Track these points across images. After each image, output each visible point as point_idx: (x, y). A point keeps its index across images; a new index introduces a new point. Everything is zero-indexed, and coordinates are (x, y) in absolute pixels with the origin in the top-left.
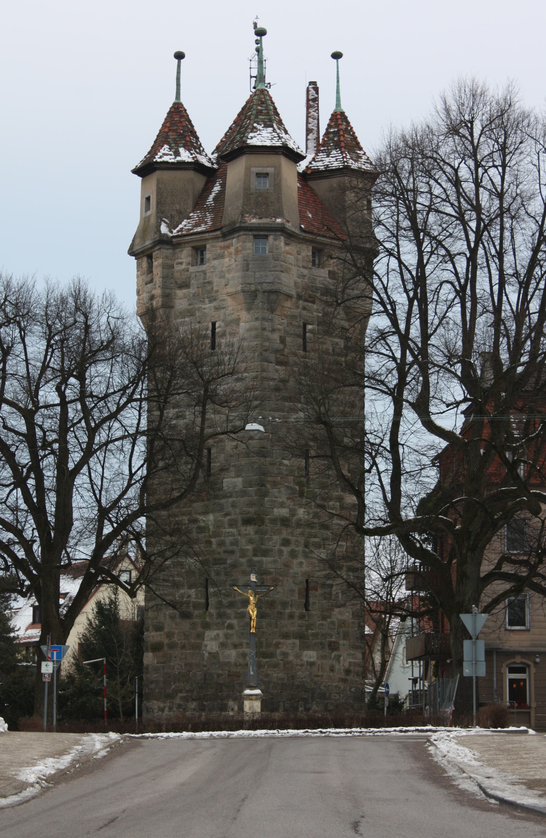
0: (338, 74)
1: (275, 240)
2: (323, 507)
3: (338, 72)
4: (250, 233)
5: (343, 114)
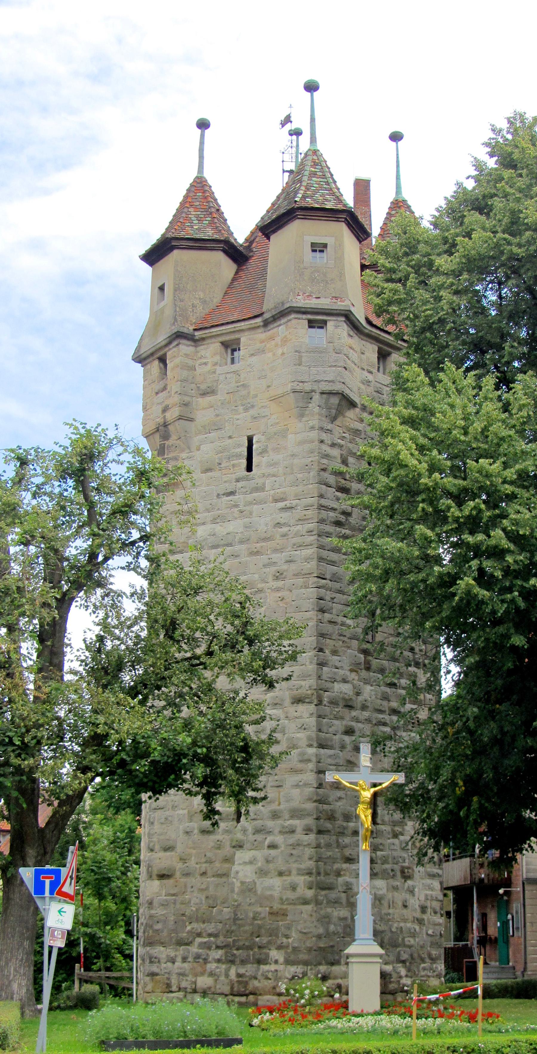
0: (397, 157)
1: (336, 327)
2: (392, 685)
3: (397, 155)
4: (304, 316)
5: (404, 201)
